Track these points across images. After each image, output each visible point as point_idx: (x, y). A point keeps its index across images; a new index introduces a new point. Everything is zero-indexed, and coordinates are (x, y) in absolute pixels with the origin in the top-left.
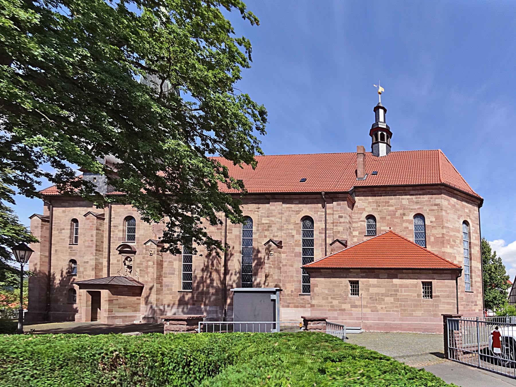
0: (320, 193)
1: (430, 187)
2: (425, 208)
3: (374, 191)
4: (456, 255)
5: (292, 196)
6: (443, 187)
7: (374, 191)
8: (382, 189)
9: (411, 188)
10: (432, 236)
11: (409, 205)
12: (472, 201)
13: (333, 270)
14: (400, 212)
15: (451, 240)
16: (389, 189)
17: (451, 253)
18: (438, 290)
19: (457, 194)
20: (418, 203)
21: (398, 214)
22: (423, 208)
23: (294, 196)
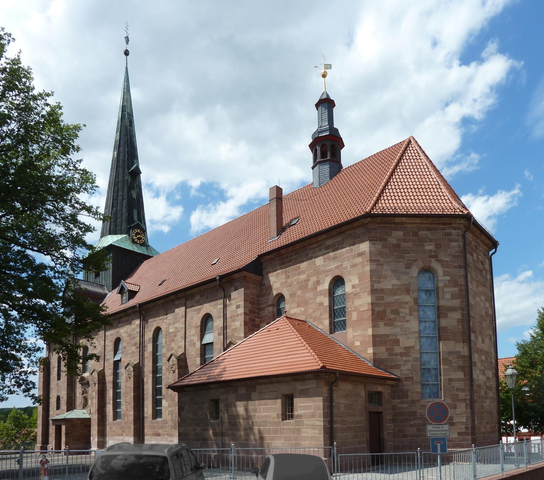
0: (214, 280)
1: (349, 226)
2: (345, 264)
3: (282, 255)
4: (398, 337)
5: (192, 290)
6: (369, 219)
7: (282, 255)
8: (290, 249)
9: (324, 236)
10: (355, 311)
11: (324, 266)
12: (444, 224)
13: (294, 377)
14: (313, 279)
15: (388, 311)
16: (282, 251)
17: (388, 336)
18: (300, 407)
19: (403, 223)
20: (336, 258)
21: (310, 284)
22: (342, 265)
23: (193, 291)
